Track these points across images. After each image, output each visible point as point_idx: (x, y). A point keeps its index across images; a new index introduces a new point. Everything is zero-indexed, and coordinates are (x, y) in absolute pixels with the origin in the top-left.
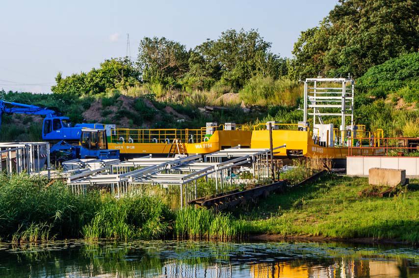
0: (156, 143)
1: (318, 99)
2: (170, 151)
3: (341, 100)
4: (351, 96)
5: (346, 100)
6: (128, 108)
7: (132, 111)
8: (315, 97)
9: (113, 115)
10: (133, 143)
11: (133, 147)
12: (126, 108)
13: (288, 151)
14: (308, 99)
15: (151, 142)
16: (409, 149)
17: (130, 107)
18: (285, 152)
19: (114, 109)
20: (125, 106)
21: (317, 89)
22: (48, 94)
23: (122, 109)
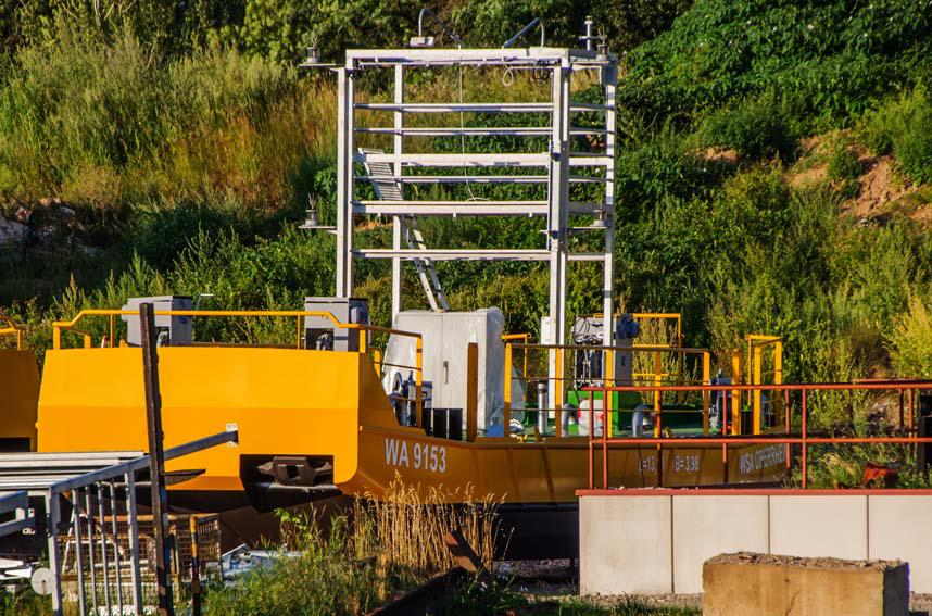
1: (418, 169)
3: (541, 170)
4: (600, 150)
5: (575, 171)
14: (359, 167)
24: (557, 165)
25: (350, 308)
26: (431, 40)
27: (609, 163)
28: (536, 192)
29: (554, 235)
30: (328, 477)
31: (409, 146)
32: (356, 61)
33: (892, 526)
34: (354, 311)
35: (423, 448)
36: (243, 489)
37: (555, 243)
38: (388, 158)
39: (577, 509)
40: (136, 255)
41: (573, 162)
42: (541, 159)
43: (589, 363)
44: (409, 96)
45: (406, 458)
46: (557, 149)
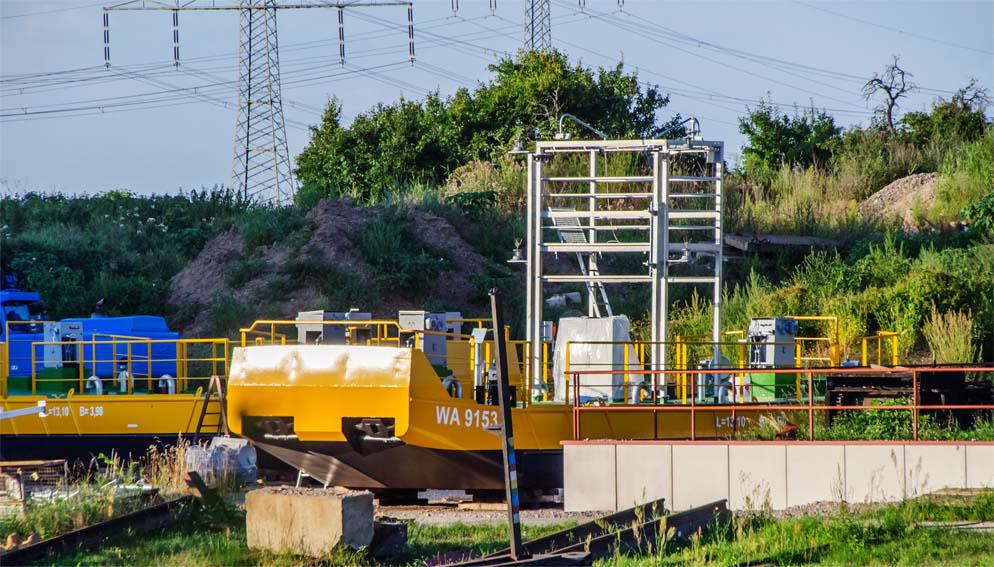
0: (171, 396)
1: (606, 222)
2: (200, 425)
3: (645, 221)
4: (712, 208)
5: (672, 222)
6: (331, 254)
7: (347, 264)
8: (592, 214)
9: (274, 278)
10: (99, 396)
11: (99, 411)
12: (321, 253)
13: (349, 425)
14: (546, 221)
15: (157, 390)
16: (833, 413)
17: (342, 250)
18: (338, 428)
19: (278, 257)
20: (321, 246)
21: (601, 179)
22: (167, 197)
23: (303, 258)
24: (656, 218)
25: (426, 318)
26: (568, 136)
27: (718, 216)
28: (643, 236)
29: (654, 266)
30: (391, 433)
31: (602, 204)
32: (543, 149)
33: (950, 467)
34: (428, 321)
35: (474, 413)
36: (345, 440)
37: (655, 271)
38: (583, 214)
39: (562, 454)
40: (752, 270)
41: (672, 215)
42: (645, 214)
43: (758, 351)
44: (600, 172)
45: (457, 419)
46: (656, 208)
